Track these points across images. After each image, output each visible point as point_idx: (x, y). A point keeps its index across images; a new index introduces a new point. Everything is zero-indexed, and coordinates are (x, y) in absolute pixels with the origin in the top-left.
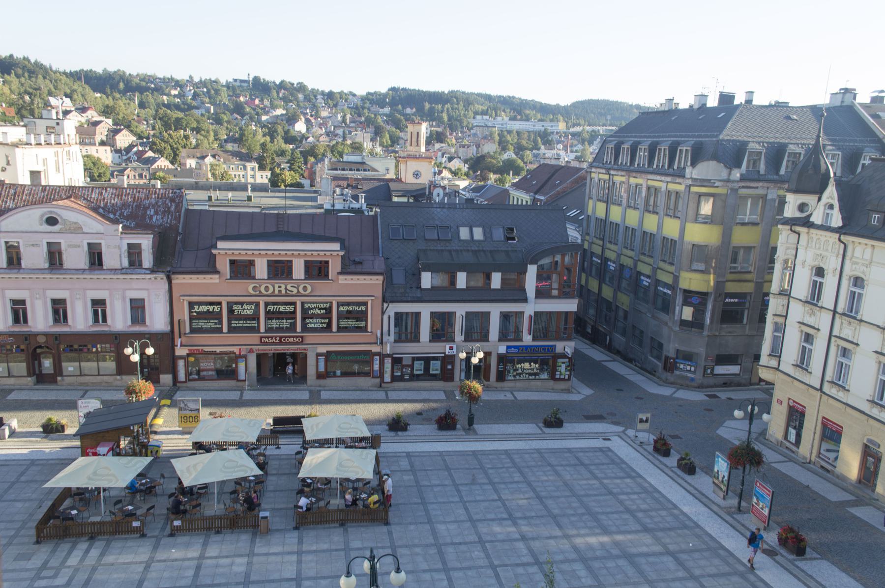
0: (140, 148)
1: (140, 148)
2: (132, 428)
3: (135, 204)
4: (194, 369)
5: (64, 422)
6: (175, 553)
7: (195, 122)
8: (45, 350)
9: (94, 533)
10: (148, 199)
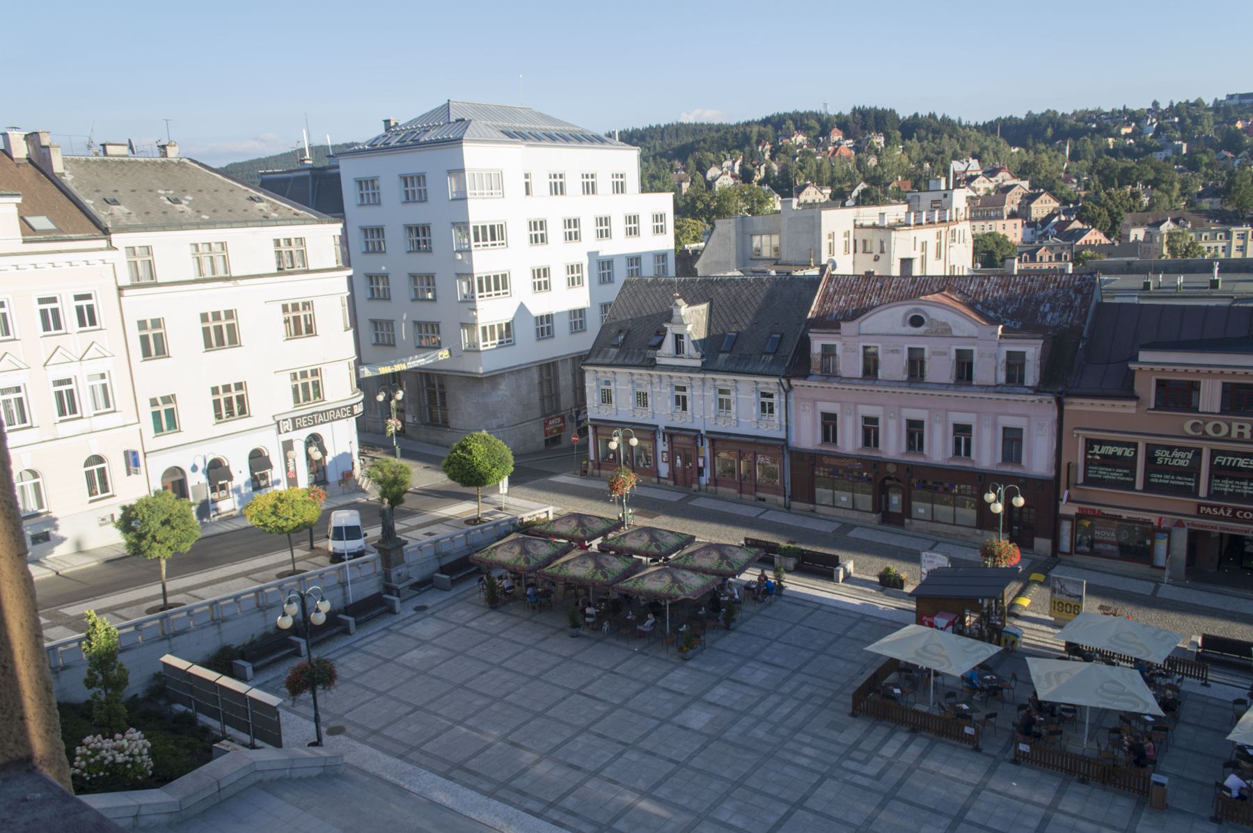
0: (1063, 218)
1: (1063, 218)
2: (980, 601)
3: (1025, 296)
4: (1085, 538)
5: (904, 576)
6: (1015, 788)
7: (1152, 171)
8: (895, 482)
9: (917, 725)
10: (1044, 289)
